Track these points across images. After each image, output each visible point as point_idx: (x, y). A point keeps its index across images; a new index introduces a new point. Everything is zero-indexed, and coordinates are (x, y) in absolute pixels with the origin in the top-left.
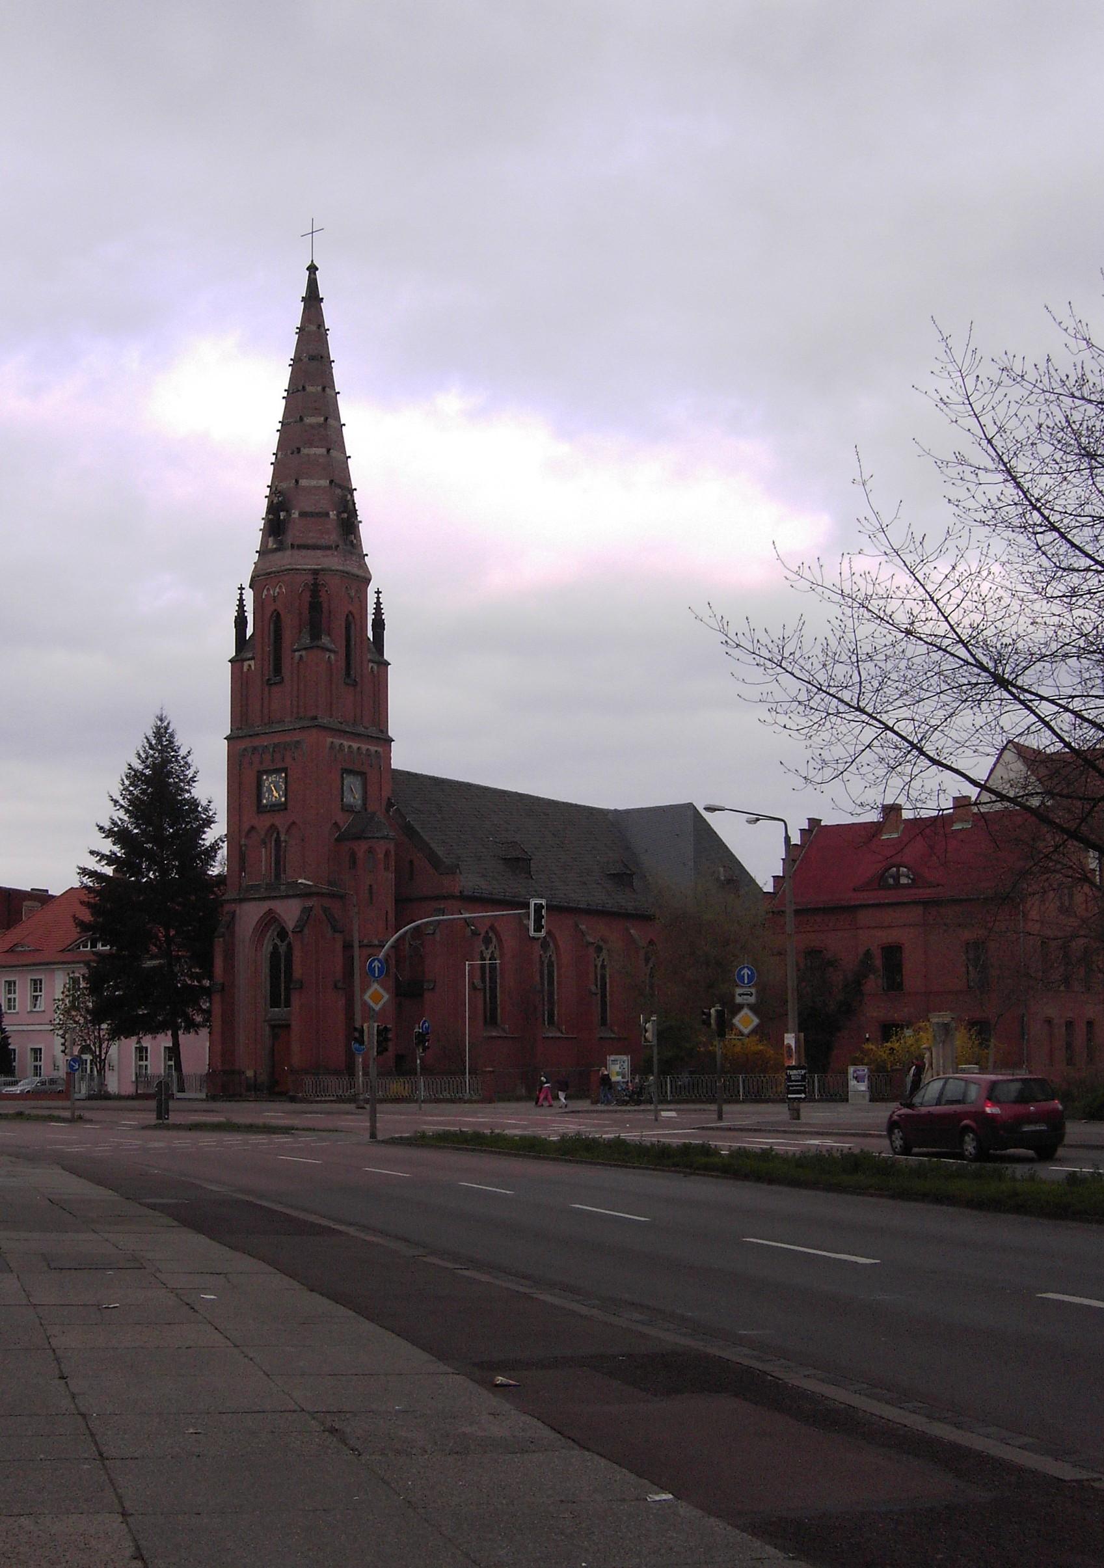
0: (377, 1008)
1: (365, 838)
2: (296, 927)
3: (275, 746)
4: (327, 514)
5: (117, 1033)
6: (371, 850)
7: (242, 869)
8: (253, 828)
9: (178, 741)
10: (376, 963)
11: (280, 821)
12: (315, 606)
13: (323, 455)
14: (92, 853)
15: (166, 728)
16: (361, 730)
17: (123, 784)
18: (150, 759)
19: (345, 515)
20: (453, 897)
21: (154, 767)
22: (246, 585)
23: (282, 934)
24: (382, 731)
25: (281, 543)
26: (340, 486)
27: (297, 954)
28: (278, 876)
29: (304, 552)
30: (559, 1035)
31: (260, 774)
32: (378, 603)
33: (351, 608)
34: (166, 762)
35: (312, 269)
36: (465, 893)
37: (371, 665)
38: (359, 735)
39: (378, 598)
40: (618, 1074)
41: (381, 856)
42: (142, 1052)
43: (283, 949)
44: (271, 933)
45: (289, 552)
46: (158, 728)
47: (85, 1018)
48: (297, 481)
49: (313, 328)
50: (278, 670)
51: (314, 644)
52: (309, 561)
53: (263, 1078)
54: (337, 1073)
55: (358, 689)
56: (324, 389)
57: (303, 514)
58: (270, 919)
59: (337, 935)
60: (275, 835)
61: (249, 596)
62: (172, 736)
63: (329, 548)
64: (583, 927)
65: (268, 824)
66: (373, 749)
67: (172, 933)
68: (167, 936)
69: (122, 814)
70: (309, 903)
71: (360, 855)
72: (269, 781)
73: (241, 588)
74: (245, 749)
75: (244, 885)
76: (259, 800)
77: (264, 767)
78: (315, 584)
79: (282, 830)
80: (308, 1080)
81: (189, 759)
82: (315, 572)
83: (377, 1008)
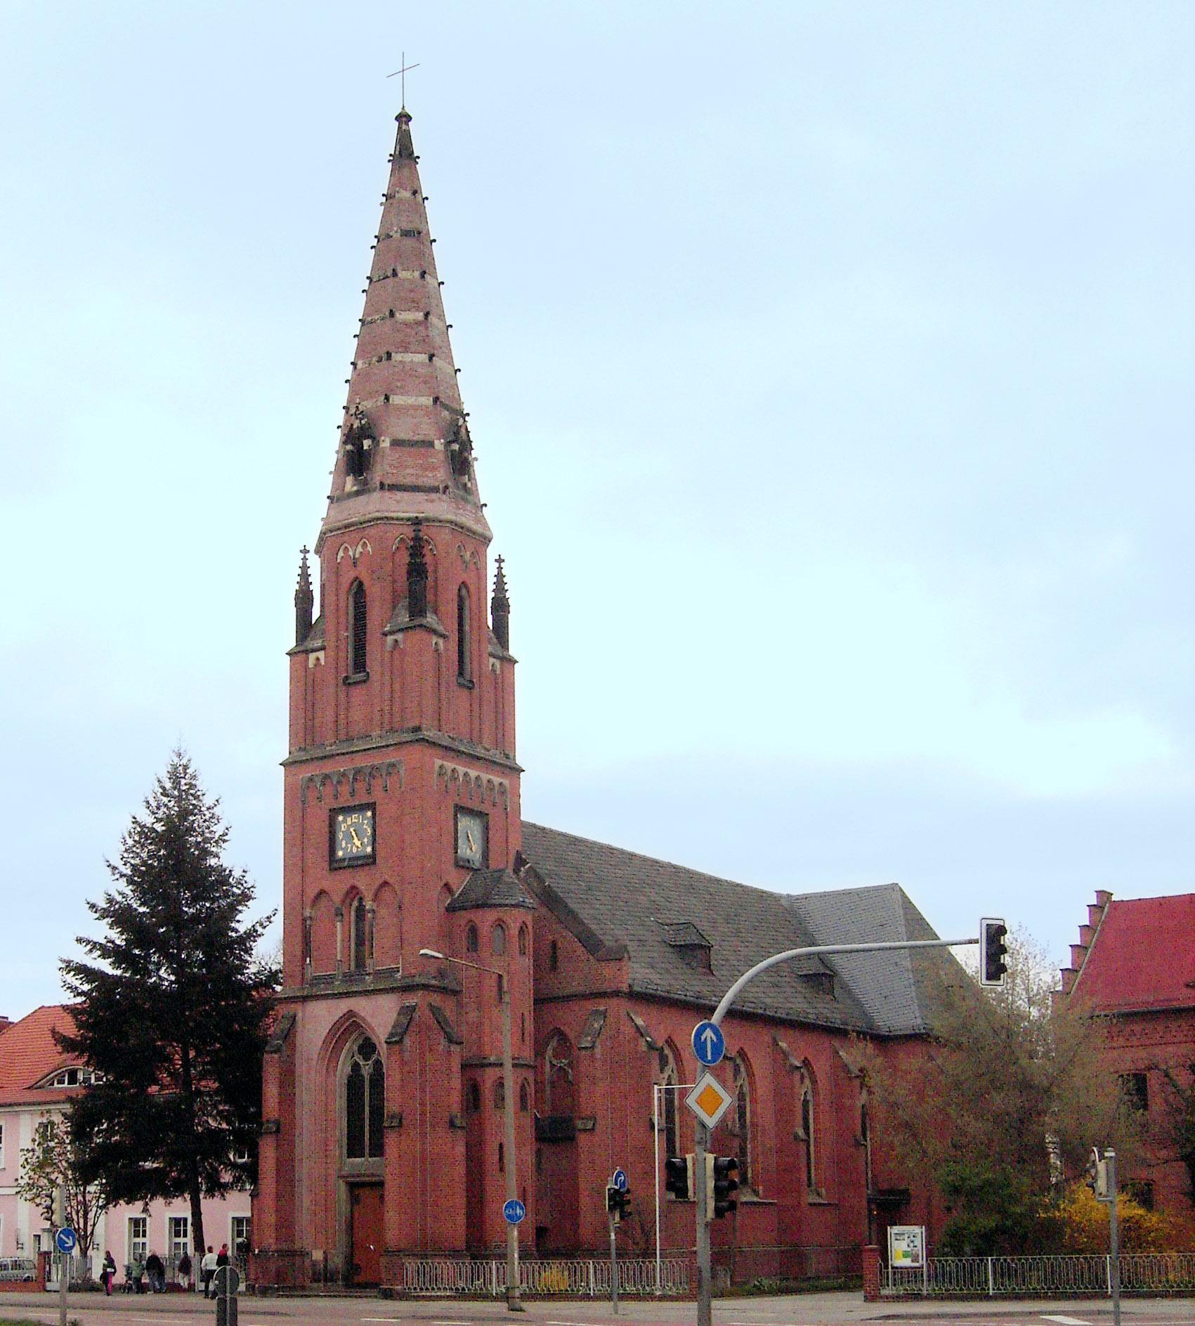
0: (711, 1122)
1: (490, 906)
2: (391, 1035)
3: (358, 771)
4: (431, 444)
5: (114, 1195)
6: (500, 924)
7: (306, 952)
8: (322, 892)
9: (201, 784)
10: (708, 1034)
11: (365, 881)
12: (417, 571)
13: (423, 364)
14: (79, 940)
15: (186, 767)
16: (480, 752)
17: (125, 843)
18: (163, 809)
19: (456, 447)
20: (616, 994)
21: (168, 820)
22: (312, 547)
23: (367, 1048)
24: (507, 757)
25: (365, 483)
26: (446, 407)
27: (392, 1081)
28: (360, 963)
29: (399, 495)
30: (755, 1199)
31: (334, 812)
32: (500, 576)
34: (184, 814)
35: (403, 118)
36: (637, 989)
37: (492, 660)
38: (479, 758)
39: (500, 568)
40: (906, 1255)
41: (515, 932)
42: (138, 1226)
43: (367, 1070)
44: (351, 1046)
45: (376, 495)
46: (175, 767)
47: (66, 1176)
48: (387, 398)
49: (406, 194)
50: (360, 663)
51: (417, 622)
52: (405, 506)
53: (338, 1261)
54: (454, 1254)
55: (476, 691)
56: (423, 274)
57: (396, 443)
58: (350, 1026)
59: (454, 1048)
60: (355, 903)
61: (315, 563)
62: (194, 777)
63: (435, 490)
64: (783, 1045)
65: (346, 887)
66: (497, 780)
67: (192, 1054)
68: (185, 1057)
69: (122, 885)
70: (412, 1000)
71: (485, 930)
72: (346, 823)
73: (305, 551)
74: (311, 779)
75: (308, 976)
76: (374, 815)
78: (417, 539)
80: (411, 1265)
81: (217, 811)
82: (417, 522)
83: (711, 1122)
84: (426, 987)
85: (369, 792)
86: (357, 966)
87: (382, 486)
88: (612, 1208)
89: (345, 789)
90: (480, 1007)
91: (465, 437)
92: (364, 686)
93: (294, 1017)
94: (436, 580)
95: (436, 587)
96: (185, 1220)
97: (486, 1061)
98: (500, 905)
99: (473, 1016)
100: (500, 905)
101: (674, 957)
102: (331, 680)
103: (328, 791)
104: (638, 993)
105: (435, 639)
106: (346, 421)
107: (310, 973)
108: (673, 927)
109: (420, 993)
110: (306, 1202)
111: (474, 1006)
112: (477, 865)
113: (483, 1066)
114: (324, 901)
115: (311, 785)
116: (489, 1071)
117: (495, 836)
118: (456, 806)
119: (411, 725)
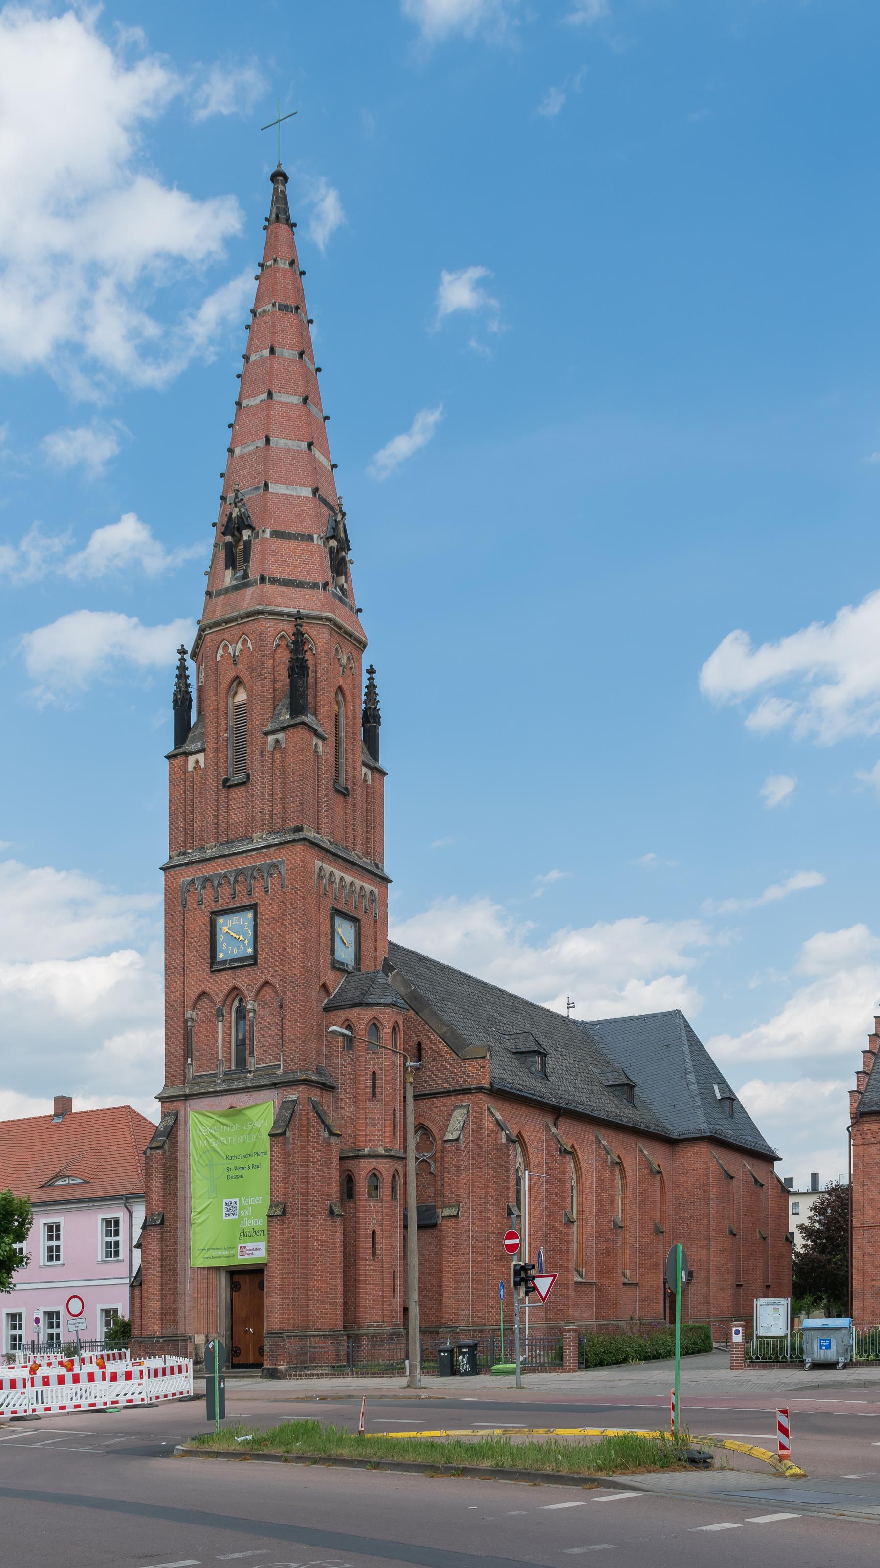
1: (368, 1005)
3: (239, 872)
6: (375, 1025)
8: (204, 994)
11: (244, 981)
12: (299, 669)
19: (333, 543)
24: (377, 867)
25: (245, 576)
28: (241, 1062)
33: (341, 682)
36: (496, 1086)
37: (364, 770)
38: (353, 864)
39: (371, 679)
41: (388, 1030)
51: (298, 720)
55: (351, 797)
65: (227, 988)
71: (361, 1028)
72: (226, 925)
73: (183, 652)
74: (192, 882)
75: (190, 1076)
77: (222, 905)
78: (298, 634)
79: (249, 995)
84: (308, 1082)
85: (250, 893)
86: (237, 1064)
87: (263, 579)
88: (517, 1284)
89: (225, 892)
90: (355, 1102)
91: (342, 535)
92: (243, 788)
93: (177, 1114)
94: (316, 680)
95: (315, 688)
96: (58, 1313)
97: (360, 1154)
98: (378, 1004)
99: (348, 1111)
100: (378, 1004)
101: (515, 1061)
102: (211, 783)
103: (208, 894)
104: (499, 1090)
105: (315, 740)
106: (223, 514)
107: (191, 1072)
108: (513, 1036)
109: (301, 1088)
110: (189, 1288)
111: (350, 1101)
112: (351, 968)
113: (357, 1157)
114: (205, 1002)
115: (192, 888)
116: (363, 1162)
117: (367, 944)
118: (333, 908)
119: (293, 825)
